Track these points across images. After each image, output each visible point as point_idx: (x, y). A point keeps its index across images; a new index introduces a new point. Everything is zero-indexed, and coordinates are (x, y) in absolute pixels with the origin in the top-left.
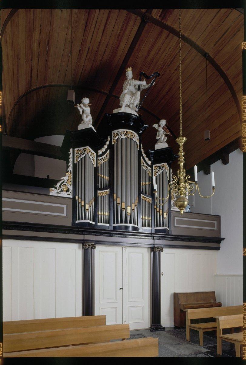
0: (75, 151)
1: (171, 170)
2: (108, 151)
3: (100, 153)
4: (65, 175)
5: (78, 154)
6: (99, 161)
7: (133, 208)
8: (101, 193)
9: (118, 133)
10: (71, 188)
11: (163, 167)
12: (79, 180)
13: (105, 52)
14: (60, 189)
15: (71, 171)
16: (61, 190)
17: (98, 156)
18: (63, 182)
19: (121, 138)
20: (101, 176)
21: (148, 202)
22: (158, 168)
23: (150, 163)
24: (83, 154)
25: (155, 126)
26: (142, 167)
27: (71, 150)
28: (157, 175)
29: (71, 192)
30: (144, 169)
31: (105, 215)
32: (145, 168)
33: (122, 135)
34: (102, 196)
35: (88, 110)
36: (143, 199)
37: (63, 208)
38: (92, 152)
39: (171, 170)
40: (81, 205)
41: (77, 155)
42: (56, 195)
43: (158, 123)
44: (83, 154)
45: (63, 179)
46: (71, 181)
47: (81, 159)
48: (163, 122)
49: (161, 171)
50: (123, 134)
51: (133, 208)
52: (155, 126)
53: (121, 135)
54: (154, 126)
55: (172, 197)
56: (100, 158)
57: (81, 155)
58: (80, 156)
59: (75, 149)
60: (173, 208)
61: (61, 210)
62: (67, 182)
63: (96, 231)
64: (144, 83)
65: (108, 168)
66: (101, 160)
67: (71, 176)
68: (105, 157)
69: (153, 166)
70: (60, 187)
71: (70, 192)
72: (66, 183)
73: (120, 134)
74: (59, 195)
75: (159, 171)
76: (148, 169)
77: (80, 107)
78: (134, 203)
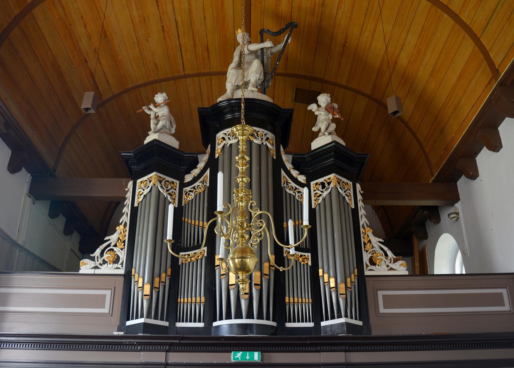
1: (358, 186)
2: (208, 172)
3: (188, 178)
5: (317, 191)
6: (186, 194)
7: (163, 280)
9: (224, 136)
10: (123, 256)
11: (329, 184)
13: (205, 18)
15: (126, 224)
16: (104, 260)
17: (183, 185)
18: (109, 245)
19: (228, 145)
20: (190, 221)
21: (302, 263)
22: (320, 188)
23: (302, 179)
24: (326, 190)
25: (313, 107)
26: (286, 191)
27: (130, 184)
28: (320, 201)
29: (122, 264)
30: (290, 194)
31: (289, 302)
32: (291, 192)
35: (163, 111)
37: (501, 294)
38: (343, 182)
39: (358, 186)
40: (228, 285)
41: (315, 192)
42: (92, 272)
44: (326, 190)
45: (109, 240)
46: (124, 242)
47: (324, 199)
48: (323, 99)
49: (326, 193)
51: (353, 280)
53: (229, 138)
54: (309, 108)
55: (365, 244)
56: (188, 189)
57: (144, 190)
58: (321, 193)
59: (139, 181)
62: (115, 246)
63: (291, 336)
65: (206, 204)
66: (190, 191)
68: (200, 184)
70: (102, 254)
72: (114, 246)
73: (226, 138)
74: (97, 272)
75: (322, 192)
77: (150, 109)
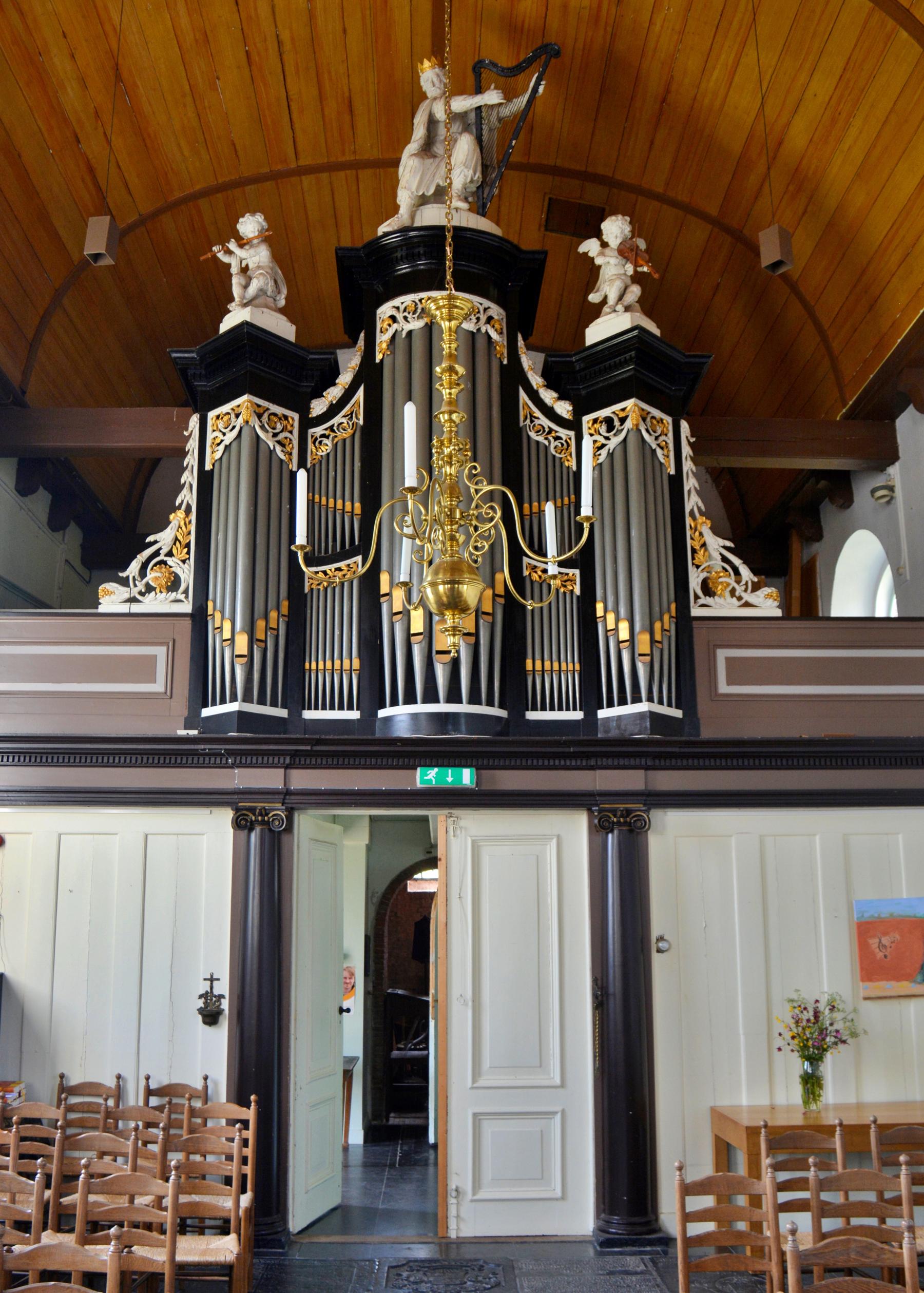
0: (210, 423)
1: (685, 426)
3: (318, 407)
4: (163, 525)
5: (597, 437)
6: (314, 443)
8: (321, 575)
9: (394, 312)
10: (187, 574)
11: (623, 420)
12: (271, 553)
14: (141, 586)
17: (307, 423)
18: (157, 553)
19: (404, 334)
22: (603, 429)
23: (564, 409)
25: (590, 247)
26: (529, 437)
29: (186, 592)
30: (538, 442)
32: (540, 439)
33: (410, 316)
34: (326, 589)
35: (259, 257)
36: (535, 577)
39: (685, 426)
42: (125, 608)
43: (598, 234)
44: (615, 435)
45: (156, 542)
46: (188, 545)
48: (615, 228)
50: (414, 313)
52: (590, 247)
53: (405, 318)
54: (582, 248)
55: (694, 551)
56: (319, 430)
57: (224, 434)
59: (212, 414)
60: (703, 606)
61: (143, 669)
62: (170, 554)
64: (492, 97)
65: (357, 464)
66: (323, 436)
67: (325, 573)
68: (344, 420)
69: (587, 419)
71: (183, 587)
72: (166, 555)
73: (400, 317)
74: (136, 608)
75: (607, 438)
76: (557, 438)
77: (229, 252)
78: (620, 642)
